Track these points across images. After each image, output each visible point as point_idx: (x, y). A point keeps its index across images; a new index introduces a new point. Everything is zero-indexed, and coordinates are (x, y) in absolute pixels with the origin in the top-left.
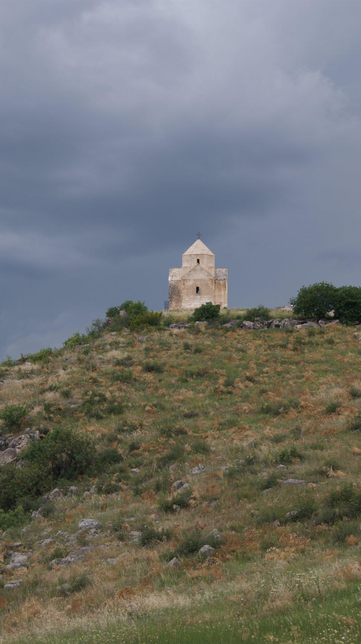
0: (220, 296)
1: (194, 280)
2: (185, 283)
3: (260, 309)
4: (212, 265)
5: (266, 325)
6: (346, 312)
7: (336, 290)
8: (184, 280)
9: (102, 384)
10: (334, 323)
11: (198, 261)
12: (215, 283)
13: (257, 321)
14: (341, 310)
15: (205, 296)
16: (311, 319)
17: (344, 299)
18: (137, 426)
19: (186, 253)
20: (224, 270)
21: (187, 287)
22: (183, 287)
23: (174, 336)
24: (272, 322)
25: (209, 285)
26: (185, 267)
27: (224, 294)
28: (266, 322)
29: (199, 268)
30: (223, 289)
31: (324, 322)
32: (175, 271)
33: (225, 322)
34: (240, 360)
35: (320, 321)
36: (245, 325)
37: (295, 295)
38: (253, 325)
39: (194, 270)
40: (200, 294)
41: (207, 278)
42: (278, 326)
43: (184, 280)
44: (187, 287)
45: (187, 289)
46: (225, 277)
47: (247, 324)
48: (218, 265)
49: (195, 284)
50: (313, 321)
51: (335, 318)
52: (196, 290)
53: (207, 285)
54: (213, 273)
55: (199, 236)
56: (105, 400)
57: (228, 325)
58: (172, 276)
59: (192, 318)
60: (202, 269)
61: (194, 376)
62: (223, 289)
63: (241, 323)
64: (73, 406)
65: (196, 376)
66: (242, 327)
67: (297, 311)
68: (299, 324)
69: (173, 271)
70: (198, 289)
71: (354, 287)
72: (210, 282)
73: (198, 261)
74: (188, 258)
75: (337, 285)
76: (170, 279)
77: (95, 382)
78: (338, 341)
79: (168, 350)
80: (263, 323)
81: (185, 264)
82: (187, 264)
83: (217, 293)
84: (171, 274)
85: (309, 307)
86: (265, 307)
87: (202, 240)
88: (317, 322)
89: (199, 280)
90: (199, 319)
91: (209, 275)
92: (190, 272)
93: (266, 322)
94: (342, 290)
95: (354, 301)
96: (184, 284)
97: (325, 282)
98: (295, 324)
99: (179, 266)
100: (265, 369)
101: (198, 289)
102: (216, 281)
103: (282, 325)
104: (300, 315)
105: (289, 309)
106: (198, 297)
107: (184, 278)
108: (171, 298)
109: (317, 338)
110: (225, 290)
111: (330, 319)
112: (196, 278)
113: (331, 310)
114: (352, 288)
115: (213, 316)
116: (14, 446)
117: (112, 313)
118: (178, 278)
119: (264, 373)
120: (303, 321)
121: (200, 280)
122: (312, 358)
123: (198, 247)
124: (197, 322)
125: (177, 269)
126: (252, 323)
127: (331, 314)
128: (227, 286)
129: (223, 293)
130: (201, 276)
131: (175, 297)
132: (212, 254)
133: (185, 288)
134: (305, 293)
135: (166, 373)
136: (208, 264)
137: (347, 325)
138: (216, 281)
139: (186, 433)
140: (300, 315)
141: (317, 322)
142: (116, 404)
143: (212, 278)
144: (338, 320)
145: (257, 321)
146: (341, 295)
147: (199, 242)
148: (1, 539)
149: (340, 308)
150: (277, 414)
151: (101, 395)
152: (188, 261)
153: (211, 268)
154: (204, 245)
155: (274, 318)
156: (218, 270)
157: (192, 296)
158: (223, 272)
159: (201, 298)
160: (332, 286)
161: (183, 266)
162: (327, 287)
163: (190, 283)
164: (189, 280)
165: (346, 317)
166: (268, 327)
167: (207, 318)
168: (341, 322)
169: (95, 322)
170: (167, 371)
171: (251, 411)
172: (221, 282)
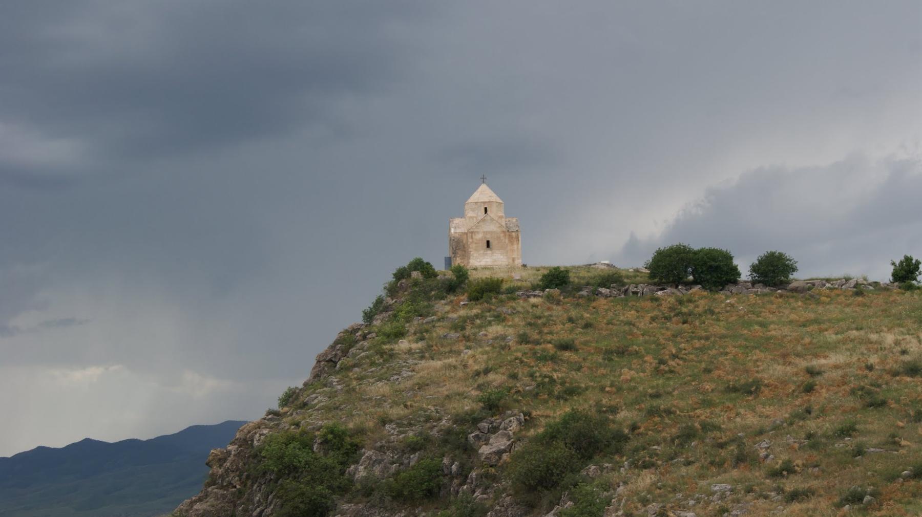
0: (513, 251)
4: (501, 214)
6: (709, 277)
7: (695, 253)
10: (696, 289)
11: (486, 209)
17: (705, 263)
19: (469, 201)
26: (471, 217)
29: (489, 218)
32: (457, 221)
33: (579, 289)
36: (601, 293)
39: (483, 220)
40: (491, 250)
41: (499, 230)
42: (635, 293)
43: (472, 233)
51: (695, 283)
52: (485, 245)
53: (499, 238)
55: (483, 180)
60: (492, 220)
63: (596, 290)
67: (652, 275)
70: (488, 242)
73: (486, 209)
75: (696, 247)
76: (453, 231)
81: (470, 214)
82: (473, 214)
87: (488, 185)
89: (489, 232)
91: (501, 226)
99: (462, 215)
101: (488, 242)
104: (656, 280)
106: (489, 252)
108: (454, 253)
116: (505, 429)
120: (661, 286)
121: (491, 233)
123: (484, 194)
129: (515, 246)
130: (492, 227)
131: (460, 252)
139: (674, 413)
140: (656, 280)
142: (567, 385)
144: (700, 286)
147: (484, 187)
148: (921, 417)
150: (750, 393)
152: (473, 210)
153: (501, 217)
157: (482, 252)
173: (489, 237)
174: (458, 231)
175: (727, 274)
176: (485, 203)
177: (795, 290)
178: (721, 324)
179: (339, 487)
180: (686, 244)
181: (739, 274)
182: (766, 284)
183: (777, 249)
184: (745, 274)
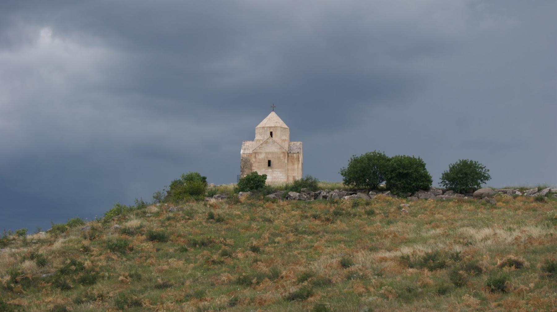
1: (266, 153)
2: (257, 156)
3: (307, 179)
5: (312, 196)
6: (398, 183)
7: (389, 160)
8: (255, 153)
9: (93, 253)
11: (271, 133)
12: (288, 156)
13: (304, 191)
14: (392, 181)
15: (276, 170)
16: (361, 190)
18: (96, 297)
19: (259, 126)
20: (298, 143)
21: (258, 160)
22: (254, 160)
23: (208, 206)
24: (320, 193)
25: (282, 158)
26: (258, 140)
27: (298, 168)
28: (313, 193)
30: (296, 163)
31: (375, 193)
32: (248, 144)
33: (269, 193)
34: (258, 229)
35: (370, 193)
36: (290, 196)
37: (346, 165)
38: (299, 196)
39: (266, 142)
40: (271, 168)
42: (325, 197)
43: (256, 153)
44: (258, 160)
45: (259, 162)
46: (299, 151)
47: (292, 195)
48: (292, 138)
49: (267, 157)
50: (364, 192)
52: (267, 164)
54: (286, 146)
56: (82, 268)
57: (272, 196)
58: (245, 149)
59: (237, 189)
60: (274, 142)
61: (197, 246)
62: (296, 163)
64: (44, 275)
65: (200, 245)
66: (287, 198)
67: (347, 182)
68: (347, 195)
69: (246, 144)
70: (269, 162)
71: (408, 157)
72: (282, 155)
73: (271, 133)
74: (261, 131)
75: (390, 154)
76: (242, 152)
77: (86, 251)
78: (378, 212)
79: (189, 219)
80: (309, 194)
81: (258, 137)
83: (290, 167)
84: (243, 147)
85: (359, 178)
86: (313, 178)
88: (368, 194)
89: (270, 153)
90: (243, 190)
91: (282, 147)
92: (261, 144)
93: (313, 193)
94: (393, 160)
95: (405, 171)
96: (255, 157)
97: (377, 152)
98: (343, 195)
99: (252, 138)
100: (278, 239)
101: (269, 162)
102: (290, 154)
103: (330, 196)
105: (339, 181)
107: (255, 151)
109: (360, 210)
110: (298, 164)
111: (382, 190)
112: (268, 151)
113: (383, 180)
114: (405, 158)
115: (257, 187)
117: (175, 184)
118: (250, 151)
119: (275, 243)
121: (272, 153)
122: (336, 228)
124: (241, 193)
125: (251, 142)
126: (298, 194)
127: (383, 185)
128: (300, 159)
129: (296, 166)
130: (272, 149)
132: (286, 127)
133: (256, 161)
134: (355, 162)
135: (169, 242)
136: (282, 137)
137: (399, 196)
138: (289, 154)
141: (368, 194)
143: (284, 151)
144: (389, 192)
145: (304, 191)
146: (393, 164)
149: (391, 178)
151: (80, 264)
152: (261, 134)
153: (284, 141)
154: (278, 118)
155: (323, 189)
156: (293, 143)
158: (297, 145)
159: (272, 171)
160: (384, 155)
161: (256, 138)
162: (380, 156)
163: (262, 156)
164: (261, 153)
165: (397, 189)
166: (315, 199)
167: (252, 188)
168: (392, 193)
169: (155, 195)
170: (172, 241)
171: (230, 282)
172: (295, 155)
173: (270, 157)
174: (247, 152)
175: (416, 180)
176: (270, 127)
177: (480, 196)
178: (378, 218)
179: (95, 300)
180: (402, 154)
181: (430, 181)
182: (455, 191)
183: (470, 157)
184: (437, 183)
